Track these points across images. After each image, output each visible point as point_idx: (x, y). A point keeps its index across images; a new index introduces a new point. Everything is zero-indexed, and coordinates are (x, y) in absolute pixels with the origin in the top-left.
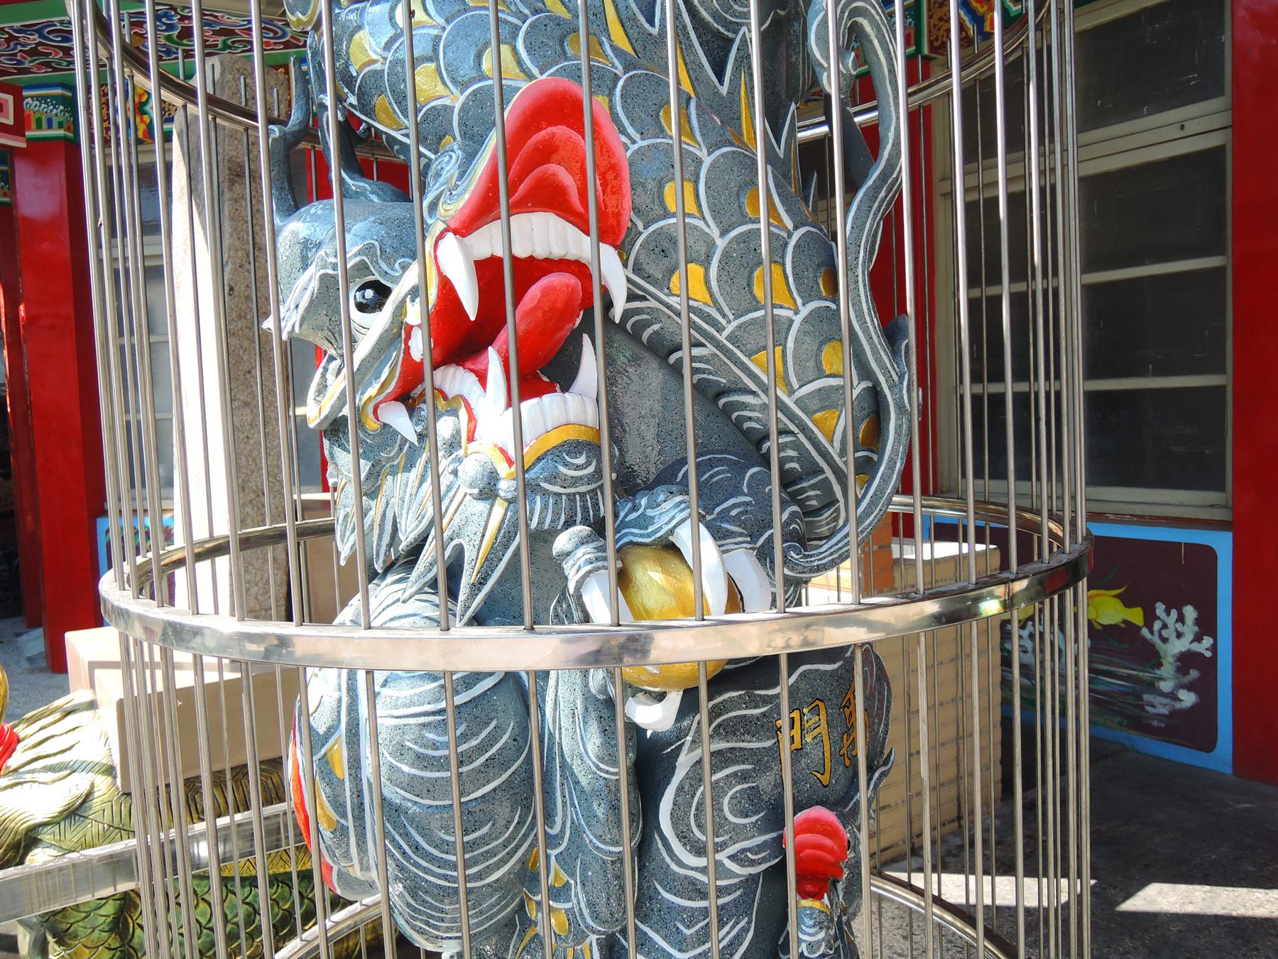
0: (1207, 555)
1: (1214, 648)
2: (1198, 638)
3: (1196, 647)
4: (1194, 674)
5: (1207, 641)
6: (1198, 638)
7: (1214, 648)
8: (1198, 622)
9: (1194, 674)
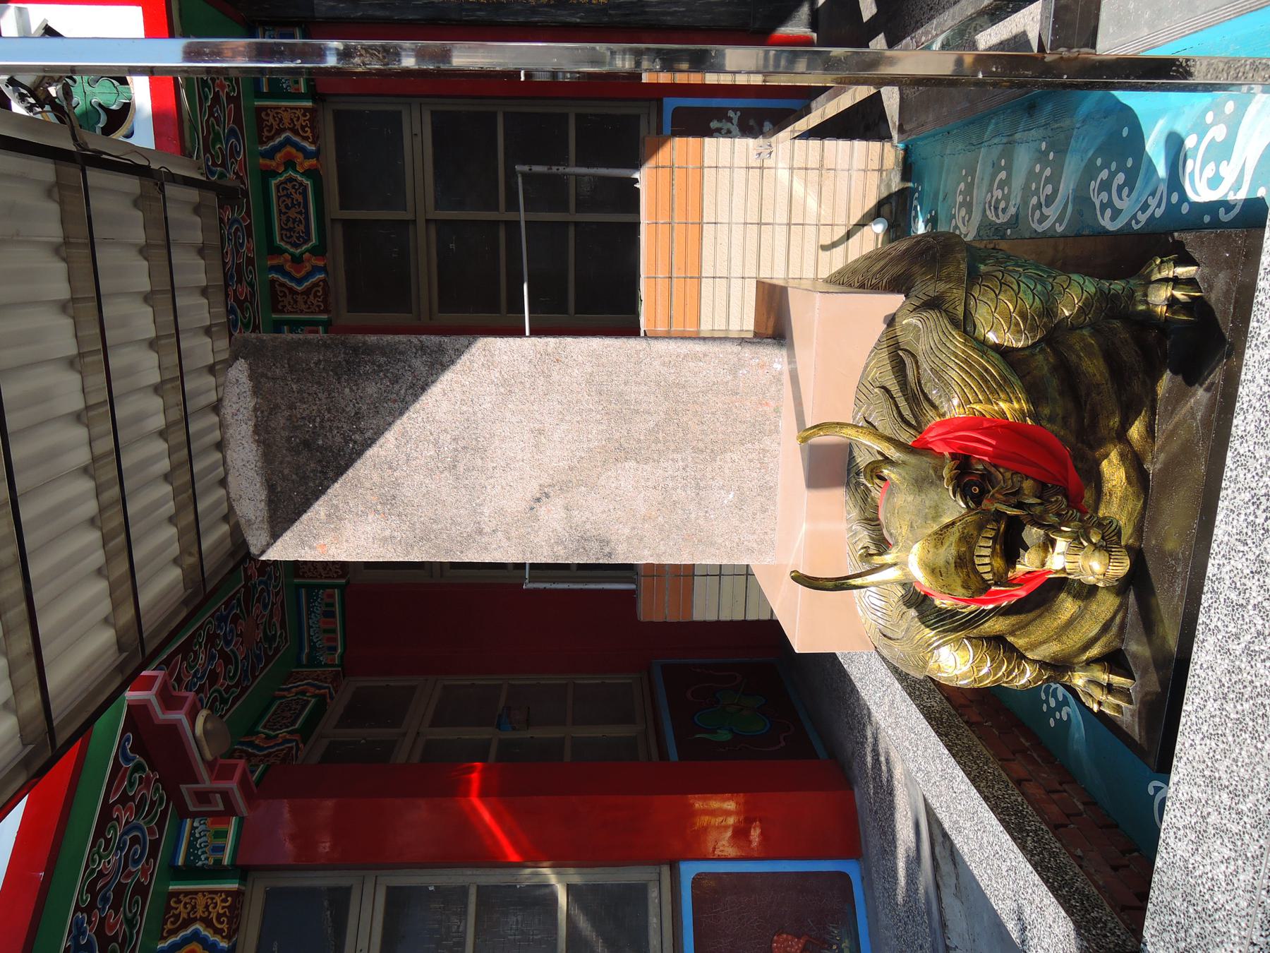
0: (677, 111)
1: (735, 110)
2: (730, 120)
3: (735, 121)
4: (752, 122)
5: (731, 114)
6: (730, 120)
7: (735, 110)
8: (720, 120)
9: (752, 122)
